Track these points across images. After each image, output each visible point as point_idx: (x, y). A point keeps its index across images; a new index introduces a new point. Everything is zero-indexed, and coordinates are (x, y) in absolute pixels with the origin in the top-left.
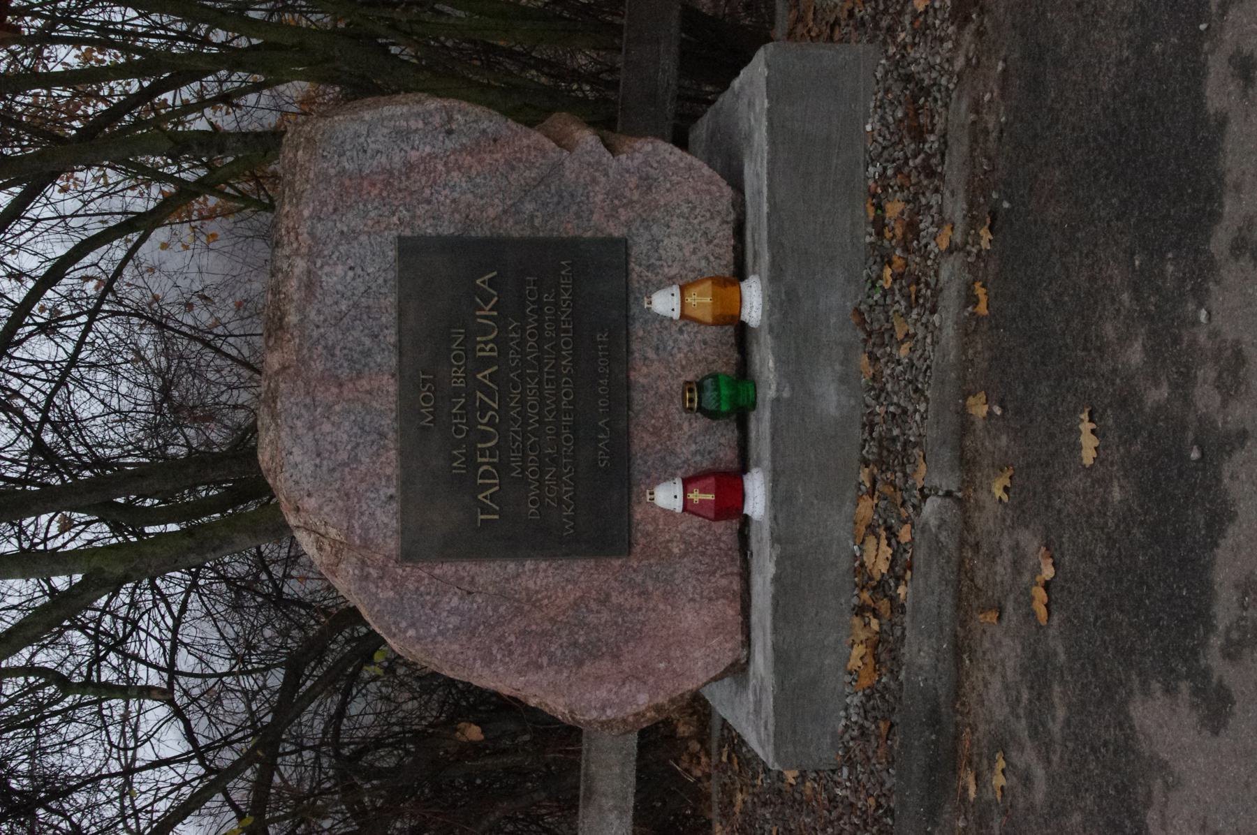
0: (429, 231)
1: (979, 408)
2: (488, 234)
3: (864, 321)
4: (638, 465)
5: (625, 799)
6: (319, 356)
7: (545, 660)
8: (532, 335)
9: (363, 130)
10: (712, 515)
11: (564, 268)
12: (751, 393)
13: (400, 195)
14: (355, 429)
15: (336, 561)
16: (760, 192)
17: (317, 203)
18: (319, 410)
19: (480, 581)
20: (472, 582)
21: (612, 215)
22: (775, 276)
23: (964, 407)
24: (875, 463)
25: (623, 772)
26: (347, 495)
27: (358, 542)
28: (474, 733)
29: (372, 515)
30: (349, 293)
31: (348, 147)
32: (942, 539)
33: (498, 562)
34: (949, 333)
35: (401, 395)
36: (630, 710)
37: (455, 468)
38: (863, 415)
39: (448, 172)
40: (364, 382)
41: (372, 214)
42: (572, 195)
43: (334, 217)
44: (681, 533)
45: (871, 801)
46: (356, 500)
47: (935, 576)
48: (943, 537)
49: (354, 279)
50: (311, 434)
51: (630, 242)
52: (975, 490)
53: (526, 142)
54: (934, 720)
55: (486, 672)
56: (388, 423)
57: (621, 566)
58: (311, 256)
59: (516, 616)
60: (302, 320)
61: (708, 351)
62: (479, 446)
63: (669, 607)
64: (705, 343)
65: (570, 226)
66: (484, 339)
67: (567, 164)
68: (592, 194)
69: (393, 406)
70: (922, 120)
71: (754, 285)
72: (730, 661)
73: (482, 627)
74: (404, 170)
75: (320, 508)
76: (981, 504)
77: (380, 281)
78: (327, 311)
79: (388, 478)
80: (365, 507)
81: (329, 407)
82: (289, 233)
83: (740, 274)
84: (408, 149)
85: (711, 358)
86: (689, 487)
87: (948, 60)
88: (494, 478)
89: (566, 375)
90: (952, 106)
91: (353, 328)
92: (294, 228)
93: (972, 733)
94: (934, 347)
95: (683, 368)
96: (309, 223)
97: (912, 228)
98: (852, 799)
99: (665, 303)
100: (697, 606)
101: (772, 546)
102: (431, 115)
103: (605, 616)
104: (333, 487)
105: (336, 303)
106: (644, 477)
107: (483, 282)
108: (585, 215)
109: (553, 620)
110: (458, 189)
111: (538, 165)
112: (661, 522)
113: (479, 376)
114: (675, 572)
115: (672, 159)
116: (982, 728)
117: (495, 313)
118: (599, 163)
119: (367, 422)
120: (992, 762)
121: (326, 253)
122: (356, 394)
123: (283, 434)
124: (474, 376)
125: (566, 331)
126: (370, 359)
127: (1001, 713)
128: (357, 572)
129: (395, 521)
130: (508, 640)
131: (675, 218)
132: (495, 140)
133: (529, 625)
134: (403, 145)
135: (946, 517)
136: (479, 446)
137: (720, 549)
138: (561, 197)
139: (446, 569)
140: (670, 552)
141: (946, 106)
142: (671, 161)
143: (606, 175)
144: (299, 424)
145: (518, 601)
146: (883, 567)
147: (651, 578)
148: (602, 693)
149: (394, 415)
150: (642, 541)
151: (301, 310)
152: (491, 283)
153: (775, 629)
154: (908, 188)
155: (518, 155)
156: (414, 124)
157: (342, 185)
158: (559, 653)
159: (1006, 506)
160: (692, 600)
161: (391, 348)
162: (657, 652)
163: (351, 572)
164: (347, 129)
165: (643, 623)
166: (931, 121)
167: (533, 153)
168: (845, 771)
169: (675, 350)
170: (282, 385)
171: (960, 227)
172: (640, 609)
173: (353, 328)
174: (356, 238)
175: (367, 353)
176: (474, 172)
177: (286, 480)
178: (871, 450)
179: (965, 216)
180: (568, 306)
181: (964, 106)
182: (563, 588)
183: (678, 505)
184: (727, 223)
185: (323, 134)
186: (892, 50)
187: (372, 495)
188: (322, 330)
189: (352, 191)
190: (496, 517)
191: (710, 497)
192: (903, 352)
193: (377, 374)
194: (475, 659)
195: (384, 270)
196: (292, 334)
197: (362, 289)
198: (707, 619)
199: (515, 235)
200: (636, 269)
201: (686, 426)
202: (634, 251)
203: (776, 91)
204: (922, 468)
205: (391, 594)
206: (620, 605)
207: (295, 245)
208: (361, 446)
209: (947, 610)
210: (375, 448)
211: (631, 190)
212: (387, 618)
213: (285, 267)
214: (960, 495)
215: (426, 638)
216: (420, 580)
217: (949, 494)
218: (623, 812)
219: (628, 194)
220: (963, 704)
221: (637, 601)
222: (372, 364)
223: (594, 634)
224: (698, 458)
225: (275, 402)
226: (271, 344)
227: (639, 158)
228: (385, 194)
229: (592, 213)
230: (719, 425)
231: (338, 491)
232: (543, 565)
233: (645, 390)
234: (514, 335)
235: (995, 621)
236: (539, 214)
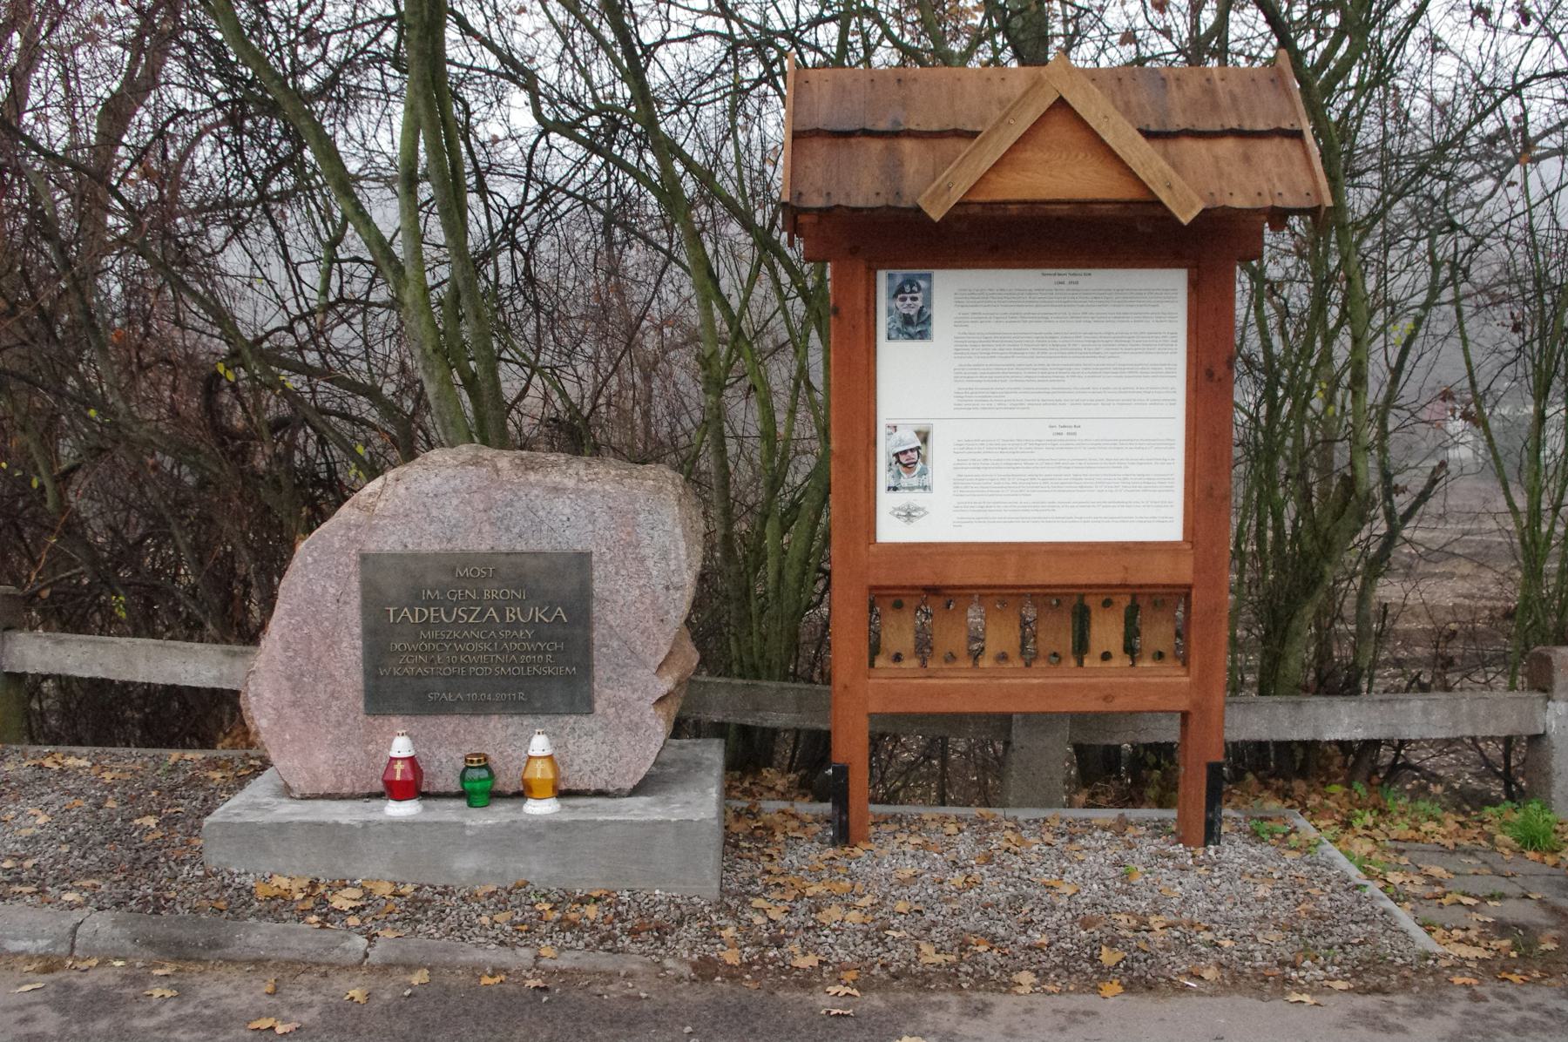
1: (419, 978)
4: (429, 721)
10: (388, 777)
16: (617, 812)
19: (347, 608)
22: (554, 826)
34: (480, 955)
36: (256, 714)
45: (173, 894)
47: (310, 946)
48: (337, 951)
54: (213, 945)
56: (459, 545)
58: (577, 491)
70: (643, 934)
81: (469, 503)
83: (563, 794)
99: (539, 745)
103: (323, 697)
115: (652, 746)
120: (171, 987)
127: (204, 994)
135: (351, 954)
139: (355, 584)
140: (368, 743)
146: (335, 905)
148: (267, 695)
151: (538, 483)
153: (302, 823)
156: (673, 563)
168: (201, 873)
175: (508, 529)
178: (426, 894)
183: (394, 754)
186: (707, 909)
191: (398, 777)
200: (572, 719)
202: (584, 719)
204: (391, 935)
209: (286, 955)
216: (347, 566)
217: (367, 955)
218: (220, 679)
221: (333, 719)
227: (652, 723)
232: (359, 653)
233: (485, 726)
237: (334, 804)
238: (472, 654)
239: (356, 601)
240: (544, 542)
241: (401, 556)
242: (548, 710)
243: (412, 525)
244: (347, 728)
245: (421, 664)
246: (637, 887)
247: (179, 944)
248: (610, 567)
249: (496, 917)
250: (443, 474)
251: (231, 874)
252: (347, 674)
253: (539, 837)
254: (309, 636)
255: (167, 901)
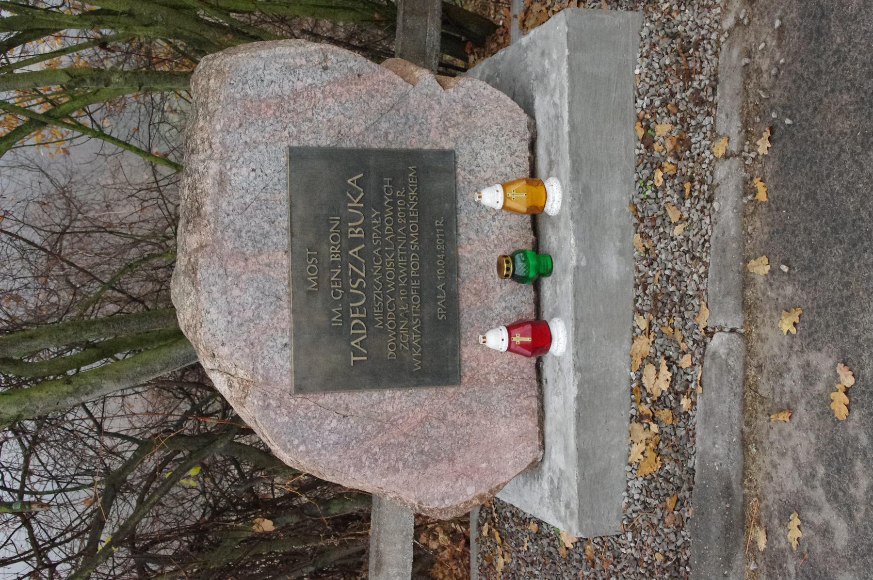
0: (311, 142)
2: (355, 145)
3: (636, 210)
4: (466, 319)
5: (405, 567)
6: (229, 237)
7: (401, 465)
8: (389, 221)
9: (261, 65)
11: (411, 171)
12: (549, 263)
13: (289, 115)
14: (258, 294)
15: (244, 395)
17: (226, 119)
18: (230, 279)
19: (352, 407)
20: (347, 409)
21: (445, 132)
23: (745, 267)
24: (651, 311)
25: (404, 547)
26: (252, 344)
27: (261, 380)
28: (268, 525)
29: (271, 359)
30: (252, 189)
31: (249, 77)
32: (730, 363)
33: (366, 393)
35: (293, 268)
36: (462, 499)
37: (335, 322)
38: (635, 278)
39: (325, 98)
40: (264, 257)
41: (268, 129)
42: (416, 118)
43: (240, 130)
44: (496, 367)
46: (259, 348)
49: (255, 178)
50: (224, 297)
51: (457, 153)
52: (757, 327)
53: (381, 77)
54: (728, 492)
55: (358, 476)
56: (283, 288)
57: (454, 393)
58: (222, 160)
59: (379, 433)
60: (216, 210)
61: (512, 234)
62: (352, 305)
63: (488, 422)
64: (510, 228)
65: (414, 141)
66: (354, 224)
67: (411, 94)
68: (429, 117)
69: (286, 275)
71: (555, 184)
72: (531, 461)
73: (354, 442)
74: (292, 96)
75: (232, 355)
76: (763, 336)
77: (275, 180)
78: (235, 202)
79: (283, 330)
80: (266, 353)
81: (237, 277)
82: (203, 142)
84: (295, 80)
85: (515, 239)
86: (513, 331)
87: (716, 22)
88: (363, 329)
89: (414, 252)
90: (722, 55)
91: (256, 216)
92: (208, 139)
93: (760, 501)
94: (712, 226)
95: (495, 246)
96: (220, 135)
97: (684, 142)
98: (637, 555)
100: (508, 420)
101: (575, 375)
102: (312, 55)
104: (241, 338)
105: (242, 197)
106: (469, 326)
107: (353, 182)
108: (425, 132)
109: (406, 435)
110: (333, 112)
111: (390, 94)
112: (482, 359)
113: (351, 252)
114: (493, 396)
115: (486, 93)
116: (771, 497)
117: (362, 205)
118: (434, 94)
119: (266, 288)
121: (234, 158)
122: (258, 266)
123: (202, 298)
124: (347, 254)
125: (413, 218)
126: (267, 239)
128: (260, 403)
129: (288, 363)
130: (374, 451)
131: (488, 136)
132: (359, 75)
133: (389, 439)
134: (291, 77)
136: (352, 305)
137: (523, 378)
138: (408, 119)
139: (327, 399)
141: (716, 54)
142: (485, 94)
143: (440, 103)
144: (214, 289)
145: (380, 421)
147: (476, 401)
149: (287, 282)
150: (469, 374)
151: (215, 202)
152: (358, 182)
153: (578, 435)
154: (675, 115)
155: (376, 87)
156: (298, 61)
157: (245, 106)
158: (410, 459)
159: (793, 337)
160: (505, 416)
161: (285, 231)
162: (480, 456)
163: (256, 403)
164: (248, 63)
165: (470, 435)
166: (701, 66)
167: (387, 86)
168: (630, 535)
169: (490, 233)
170: (201, 260)
171: (736, 139)
172: (468, 424)
173: (256, 216)
174: (255, 148)
175: (266, 236)
176: (343, 100)
177: (205, 333)
179: (740, 132)
180: (415, 200)
181: (735, 53)
182: (413, 411)
183: (504, 346)
184: (524, 140)
185: (231, 67)
187: (271, 344)
188: (232, 217)
189: (253, 111)
190: (365, 358)
191: (528, 339)
192: (678, 231)
193: (273, 251)
194: (349, 467)
195: (279, 172)
196: (208, 221)
197: (262, 186)
198: (515, 430)
199: (375, 146)
201: (498, 289)
202: (460, 160)
203: (575, 44)
205: (287, 419)
206: (454, 422)
207: (209, 152)
208: (262, 307)
209: (736, 414)
210: (273, 307)
211: (457, 115)
212: (283, 438)
213: (201, 168)
214: (742, 331)
215: (313, 452)
216: (308, 408)
217: (733, 331)
219: (454, 117)
220: (751, 481)
221: (465, 418)
222: (270, 244)
223: (435, 444)
224: (507, 312)
225: (195, 273)
226: (190, 228)
227: (463, 91)
228: (278, 114)
229: (430, 131)
230: (521, 287)
231: (245, 341)
232: (398, 393)
234: (376, 221)
235: (787, 420)
236: (391, 131)
237: (549, 414)
238: (397, 274)
239: (345, 398)
240: (279, 197)
241: (297, 349)
242: (452, 196)
243: (263, 338)
244: (474, 404)
245: (409, 327)
246: (632, 93)
247: (728, 528)
248: (304, 127)
249: (675, 219)
250: (207, 305)
251: (629, 504)
252: (421, 405)
253: (586, 190)
254: (383, 446)
255: (667, 559)
